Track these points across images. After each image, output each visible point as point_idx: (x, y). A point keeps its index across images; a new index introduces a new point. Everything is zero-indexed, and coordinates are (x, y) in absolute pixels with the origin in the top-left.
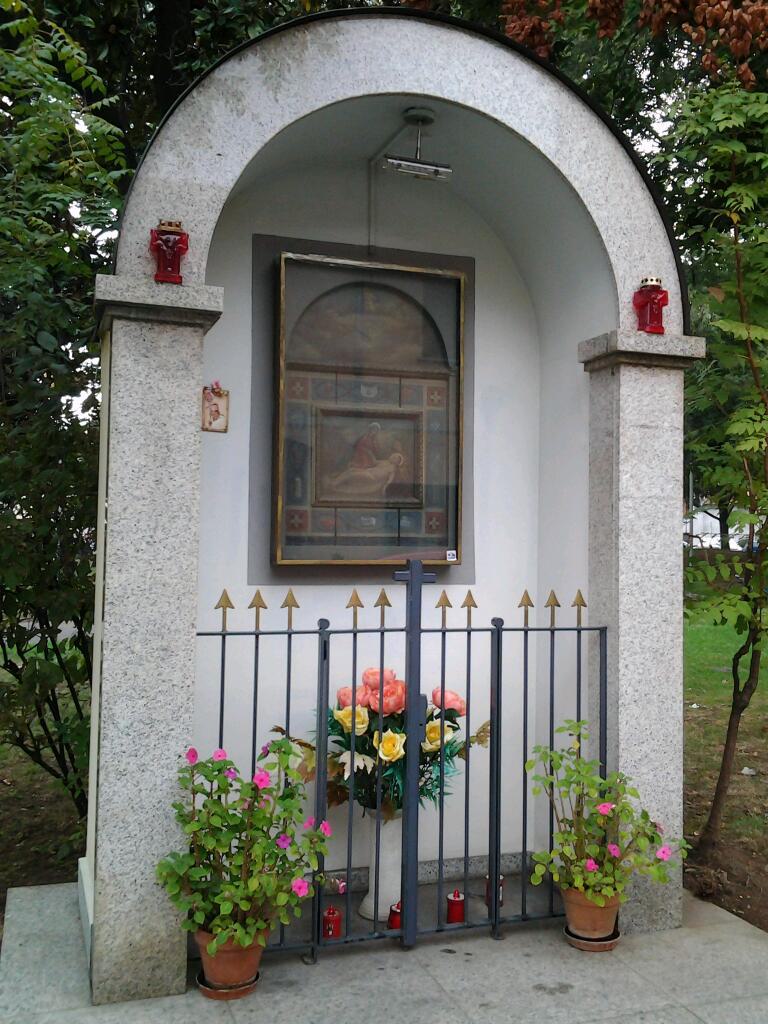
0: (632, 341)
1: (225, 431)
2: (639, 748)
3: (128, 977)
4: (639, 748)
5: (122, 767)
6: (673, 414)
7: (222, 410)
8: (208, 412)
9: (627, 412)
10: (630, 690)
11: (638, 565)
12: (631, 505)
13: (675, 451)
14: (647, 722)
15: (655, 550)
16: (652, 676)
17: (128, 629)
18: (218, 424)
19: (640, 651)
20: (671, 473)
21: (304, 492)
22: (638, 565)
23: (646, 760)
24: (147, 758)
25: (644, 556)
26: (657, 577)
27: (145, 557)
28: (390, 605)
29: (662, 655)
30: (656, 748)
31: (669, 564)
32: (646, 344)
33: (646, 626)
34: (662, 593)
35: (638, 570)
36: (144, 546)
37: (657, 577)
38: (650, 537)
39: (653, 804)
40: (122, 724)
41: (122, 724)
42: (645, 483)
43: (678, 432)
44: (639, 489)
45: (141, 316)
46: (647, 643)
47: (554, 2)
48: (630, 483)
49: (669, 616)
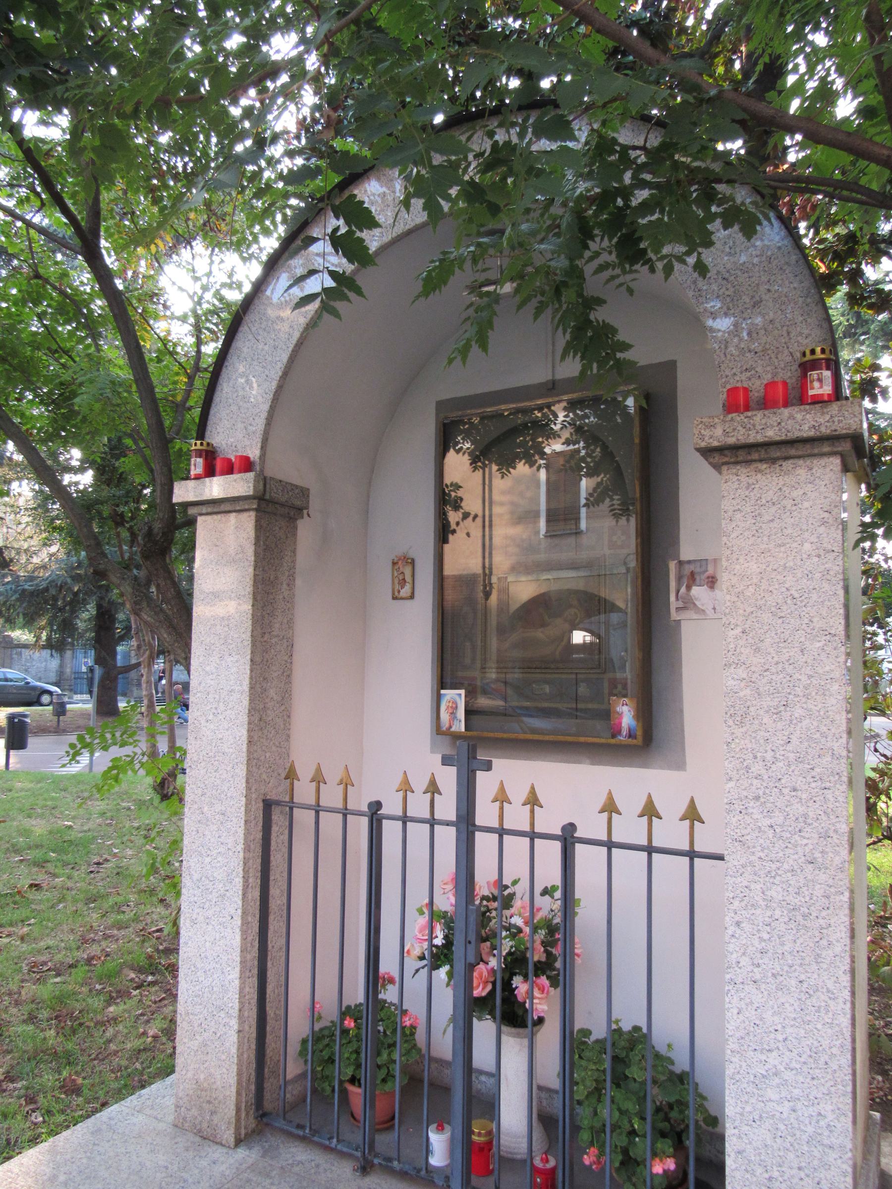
0: (719, 432)
1: (412, 597)
2: (763, 1057)
3: (195, 1112)
4: (763, 1057)
5: (194, 916)
6: (822, 530)
7: (408, 578)
8: (396, 581)
9: (734, 535)
10: (745, 961)
11: (757, 768)
12: (744, 676)
13: (826, 586)
14: (776, 1019)
15: (790, 747)
16: (786, 948)
17: (200, 791)
18: (406, 591)
19: (763, 903)
20: (818, 623)
21: (473, 660)
22: (757, 768)
23: (777, 1080)
24: (210, 912)
25: (769, 755)
26: (795, 790)
27: (212, 727)
28: (440, 794)
29: (804, 916)
30: (794, 1065)
31: (817, 770)
32: (742, 431)
33: (774, 866)
34: (806, 816)
35: (758, 777)
36: (211, 717)
37: (795, 790)
38: (780, 725)
39: (791, 1156)
40: (196, 876)
41: (196, 876)
42: (768, 641)
43: (831, 556)
44: (757, 650)
45: (210, 510)
46: (776, 893)
47: (4, 30)
48: (741, 642)
49: (818, 855)
